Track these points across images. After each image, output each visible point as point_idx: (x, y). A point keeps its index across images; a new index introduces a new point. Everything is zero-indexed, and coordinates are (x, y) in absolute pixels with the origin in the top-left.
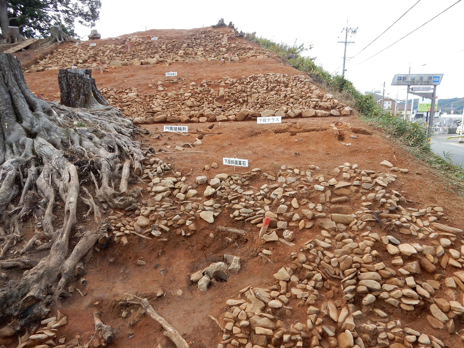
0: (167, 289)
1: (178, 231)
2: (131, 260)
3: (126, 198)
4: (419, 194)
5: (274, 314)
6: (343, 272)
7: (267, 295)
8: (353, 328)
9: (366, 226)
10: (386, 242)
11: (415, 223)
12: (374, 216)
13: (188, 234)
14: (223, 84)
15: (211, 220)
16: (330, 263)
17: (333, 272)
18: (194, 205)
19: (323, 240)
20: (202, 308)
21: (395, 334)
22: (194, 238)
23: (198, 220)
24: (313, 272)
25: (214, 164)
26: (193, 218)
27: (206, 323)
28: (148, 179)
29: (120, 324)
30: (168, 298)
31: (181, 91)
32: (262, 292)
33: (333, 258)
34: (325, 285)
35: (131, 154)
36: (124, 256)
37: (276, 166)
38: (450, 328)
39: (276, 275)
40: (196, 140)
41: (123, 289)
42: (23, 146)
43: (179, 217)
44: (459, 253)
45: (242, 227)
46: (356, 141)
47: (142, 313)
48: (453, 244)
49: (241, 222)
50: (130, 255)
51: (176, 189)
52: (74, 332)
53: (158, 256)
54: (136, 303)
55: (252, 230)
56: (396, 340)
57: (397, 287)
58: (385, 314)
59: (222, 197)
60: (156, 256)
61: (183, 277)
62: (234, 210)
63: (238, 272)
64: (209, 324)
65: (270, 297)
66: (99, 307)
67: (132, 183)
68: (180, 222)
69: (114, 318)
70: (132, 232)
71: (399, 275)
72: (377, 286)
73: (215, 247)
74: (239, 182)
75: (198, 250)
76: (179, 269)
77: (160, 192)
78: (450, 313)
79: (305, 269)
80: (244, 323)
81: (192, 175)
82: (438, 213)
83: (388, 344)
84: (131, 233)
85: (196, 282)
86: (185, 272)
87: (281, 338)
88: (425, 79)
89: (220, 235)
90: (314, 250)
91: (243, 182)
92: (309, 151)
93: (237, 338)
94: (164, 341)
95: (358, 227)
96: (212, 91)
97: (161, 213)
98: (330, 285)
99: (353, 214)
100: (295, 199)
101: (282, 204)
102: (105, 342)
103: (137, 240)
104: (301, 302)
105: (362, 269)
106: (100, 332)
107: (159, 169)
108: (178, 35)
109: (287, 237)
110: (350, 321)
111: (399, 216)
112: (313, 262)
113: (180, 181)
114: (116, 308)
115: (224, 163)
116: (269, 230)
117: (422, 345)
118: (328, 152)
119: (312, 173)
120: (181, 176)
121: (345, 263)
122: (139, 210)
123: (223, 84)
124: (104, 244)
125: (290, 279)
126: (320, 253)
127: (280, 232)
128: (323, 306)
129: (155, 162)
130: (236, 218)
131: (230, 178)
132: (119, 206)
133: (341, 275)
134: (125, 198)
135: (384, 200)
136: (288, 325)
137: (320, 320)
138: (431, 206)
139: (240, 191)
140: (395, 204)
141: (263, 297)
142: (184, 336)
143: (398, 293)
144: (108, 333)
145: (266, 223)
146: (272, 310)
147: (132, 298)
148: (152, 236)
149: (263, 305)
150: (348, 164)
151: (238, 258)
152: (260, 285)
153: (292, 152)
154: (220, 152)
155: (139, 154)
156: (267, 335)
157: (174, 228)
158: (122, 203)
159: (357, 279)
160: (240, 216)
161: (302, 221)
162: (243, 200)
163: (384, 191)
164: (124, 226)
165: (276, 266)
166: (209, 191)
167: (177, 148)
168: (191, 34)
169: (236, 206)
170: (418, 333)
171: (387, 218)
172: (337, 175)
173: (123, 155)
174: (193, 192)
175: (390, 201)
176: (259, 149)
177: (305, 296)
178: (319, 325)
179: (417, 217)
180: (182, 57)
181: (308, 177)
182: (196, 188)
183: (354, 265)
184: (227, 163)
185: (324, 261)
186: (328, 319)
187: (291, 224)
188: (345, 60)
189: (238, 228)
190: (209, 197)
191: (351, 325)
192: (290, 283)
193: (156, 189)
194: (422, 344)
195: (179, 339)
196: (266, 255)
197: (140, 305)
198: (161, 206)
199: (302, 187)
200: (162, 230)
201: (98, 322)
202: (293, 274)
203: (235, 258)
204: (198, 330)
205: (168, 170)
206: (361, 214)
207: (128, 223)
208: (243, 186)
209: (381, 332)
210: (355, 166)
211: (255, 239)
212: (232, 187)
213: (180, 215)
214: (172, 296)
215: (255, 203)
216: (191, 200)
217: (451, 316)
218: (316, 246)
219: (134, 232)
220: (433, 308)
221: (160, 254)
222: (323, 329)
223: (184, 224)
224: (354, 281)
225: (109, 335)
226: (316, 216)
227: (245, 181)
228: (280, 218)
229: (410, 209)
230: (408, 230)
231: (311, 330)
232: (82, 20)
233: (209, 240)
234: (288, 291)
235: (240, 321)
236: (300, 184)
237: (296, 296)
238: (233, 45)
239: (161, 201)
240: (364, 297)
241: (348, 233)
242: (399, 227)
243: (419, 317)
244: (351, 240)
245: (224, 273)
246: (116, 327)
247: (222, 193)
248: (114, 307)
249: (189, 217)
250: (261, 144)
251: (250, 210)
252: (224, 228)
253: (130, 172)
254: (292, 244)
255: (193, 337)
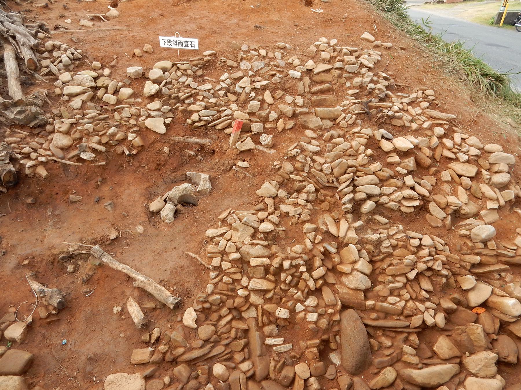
0: (121, 228)
1: (119, 149)
2: (59, 196)
3: (26, 108)
4: (406, 74)
5: (266, 239)
6: (337, 178)
7: (254, 218)
8: (356, 241)
9: (356, 119)
10: (379, 138)
11: (407, 111)
12: (363, 107)
13: (134, 152)
15: (162, 130)
16: (321, 170)
17: (326, 181)
18: (134, 110)
19: (309, 143)
20: (174, 244)
21: (397, 240)
22: (143, 155)
23: (143, 131)
24: (304, 183)
25: (147, 47)
26: (136, 129)
27: (184, 262)
28: (52, 76)
29: (68, 282)
30: (126, 239)
32: (247, 215)
33: (324, 163)
34: (319, 196)
35: (11, 36)
36: (47, 192)
37: (235, 46)
38: (449, 224)
39: (259, 192)
40: (109, 10)
41: (59, 236)
43: (116, 129)
44: (452, 142)
45: (205, 135)
46: (328, 6)
47: (97, 264)
48: (446, 132)
49: (203, 128)
50: (56, 190)
51: (100, 88)
52: (5, 305)
53: (98, 187)
54: (84, 252)
55: (218, 137)
56: (400, 246)
57: (396, 188)
58: (385, 220)
59: (170, 96)
60: (95, 186)
61: (139, 209)
62: (191, 112)
63: (210, 192)
64: (188, 262)
65: (257, 220)
66: (30, 266)
67: (28, 84)
68: (119, 136)
69: (58, 276)
70: (50, 158)
71: (397, 174)
72: (376, 190)
73: (172, 164)
74: (189, 72)
75: (151, 171)
76: (132, 199)
77: (77, 95)
78: (448, 209)
79: (294, 180)
80: (235, 256)
81: (119, 65)
82: (429, 97)
83: (392, 251)
84: (49, 160)
85: (158, 212)
86: (140, 202)
87: (281, 265)
89: (177, 148)
90: (302, 156)
91: (195, 72)
92: (271, 21)
93: (228, 274)
94: (136, 293)
95: (347, 122)
97: (87, 126)
98: (325, 194)
99: (338, 107)
100: (267, 92)
101: (253, 100)
102: (54, 309)
103: (61, 169)
104: (294, 220)
105: (359, 173)
106: (44, 299)
107: (65, 59)
109: (266, 143)
110: (352, 234)
111: (391, 104)
112: (301, 171)
113: (103, 75)
114: (56, 263)
115: (162, 45)
116: (241, 136)
117: (425, 247)
118: (296, 24)
119: (282, 54)
120: (103, 68)
121: (339, 168)
122: (52, 124)
124: (12, 180)
125: (277, 195)
126: (309, 159)
127: (256, 138)
128: (320, 221)
129: (55, 47)
130: (196, 124)
131: (175, 68)
132: (17, 122)
133: (335, 182)
134: (24, 108)
135: (371, 86)
136: (284, 249)
137: (319, 238)
138: (422, 90)
139: (194, 85)
140: (385, 89)
141: (252, 221)
142: (161, 282)
143: (398, 195)
144: (56, 298)
145: (238, 128)
146: (264, 236)
147: (76, 248)
148: (83, 161)
149: (252, 231)
150: (324, 40)
151: (208, 176)
152: (242, 206)
153: (251, 23)
154: (150, 28)
155: (25, 36)
156: (264, 266)
157: (111, 146)
158: (21, 117)
159: (353, 184)
160: (200, 120)
161: (281, 120)
162: (201, 98)
163: (371, 74)
164: (35, 150)
165: (256, 180)
166: (150, 88)
167: (83, 22)
169: (192, 107)
170: (420, 236)
171: (377, 108)
172: (313, 55)
174: (126, 91)
175: (378, 86)
176: (204, 21)
177: (298, 213)
178: (319, 243)
179: (408, 104)
181: (278, 61)
182: (129, 86)
183: (349, 170)
184: (166, 44)
185: (315, 168)
186: (328, 236)
187: (268, 126)
189: (199, 136)
190: (152, 98)
191: (354, 239)
192: (278, 199)
193: (68, 90)
194: (425, 246)
195: (155, 287)
196: (242, 168)
197: (89, 255)
198: (84, 116)
199: (274, 75)
200: (95, 151)
201: (36, 286)
202: (280, 188)
203: (203, 175)
204: (177, 273)
205: (78, 59)
206: (347, 106)
207: (40, 146)
208: (195, 78)
209: (384, 240)
210: (333, 42)
211: (224, 149)
212: (182, 80)
213: (116, 126)
214: (131, 235)
215: (217, 101)
216: (126, 103)
217: (449, 212)
218: (303, 150)
219: (53, 158)
220: (432, 206)
221: (99, 183)
222: (324, 247)
223: (125, 139)
224: (351, 188)
225: (59, 300)
226: (297, 112)
227: (197, 71)
228: (253, 119)
229: (400, 94)
230: (401, 121)
231: (311, 251)
233: (164, 156)
234: (276, 209)
235: (228, 254)
236: (271, 69)
237: (287, 213)
239: (82, 108)
240: (362, 204)
241: (336, 131)
242: (391, 118)
243: (418, 217)
244: (341, 139)
245: (191, 196)
246: (63, 286)
247: (169, 89)
248: (53, 263)
249: (129, 128)
250: (205, 12)
251: (213, 112)
252: (181, 139)
253: (19, 65)
254: (272, 151)
255: (173, 282)
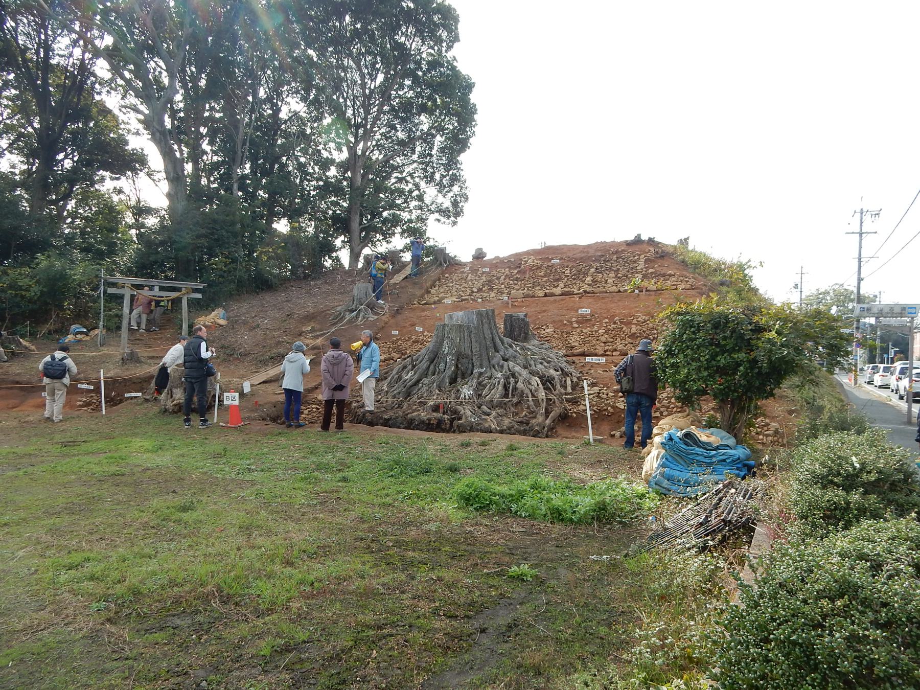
14: (635, 321)
23: (614, 407)
31: (596, 328)
42: (502, 367)
88: (897, 310)
96: (625, 328)
108: (583, 255)
123: (635, 321)
168: (599, 254)
173: (565, 374)
180: (589, 285)
188: (860, 262)
232: (439, 217)
238: (651, 270)
